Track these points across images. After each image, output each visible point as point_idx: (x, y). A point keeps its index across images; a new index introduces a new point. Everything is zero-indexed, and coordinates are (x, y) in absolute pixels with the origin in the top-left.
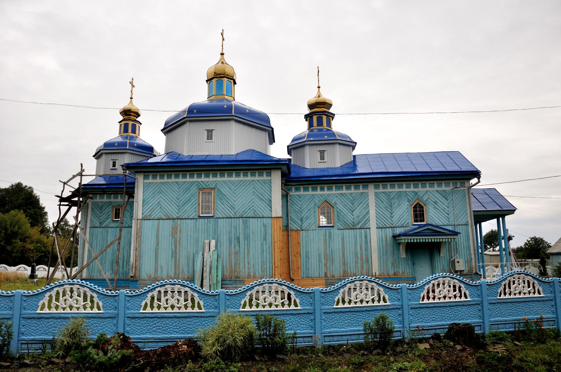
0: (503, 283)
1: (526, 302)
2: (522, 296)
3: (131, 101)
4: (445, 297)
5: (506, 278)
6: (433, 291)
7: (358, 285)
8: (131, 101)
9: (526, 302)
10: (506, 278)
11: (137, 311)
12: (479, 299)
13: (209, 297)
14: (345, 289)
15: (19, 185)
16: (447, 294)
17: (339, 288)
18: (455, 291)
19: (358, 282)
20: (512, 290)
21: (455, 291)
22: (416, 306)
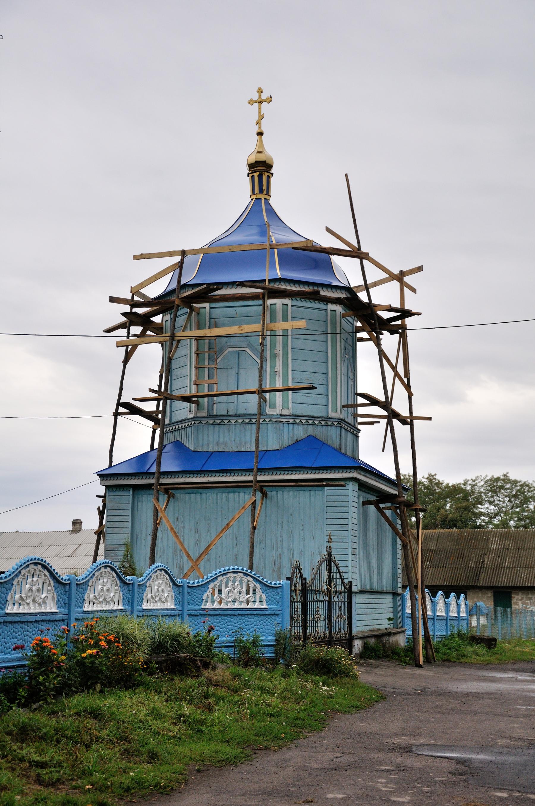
0: (211, 586)
1: (242, 615)
2: (236, 606)
3: (260, 143)
4: (234, 602)
5: (216, 578)
6: (220, 591)
7: (232, 579)
8: (260, 143)
9: (242, 615)
10: (216, 578)
11: (197, 607)
12: (279, 607)
13: (271, 590)
14: (215, 583)
15: (391, 334)
16: (237, 597)
17: (209, 583)
18: (248, 592)
19: (232, 574)
20: (223, 597)
21: (248, 592)
22: (195, 613)
